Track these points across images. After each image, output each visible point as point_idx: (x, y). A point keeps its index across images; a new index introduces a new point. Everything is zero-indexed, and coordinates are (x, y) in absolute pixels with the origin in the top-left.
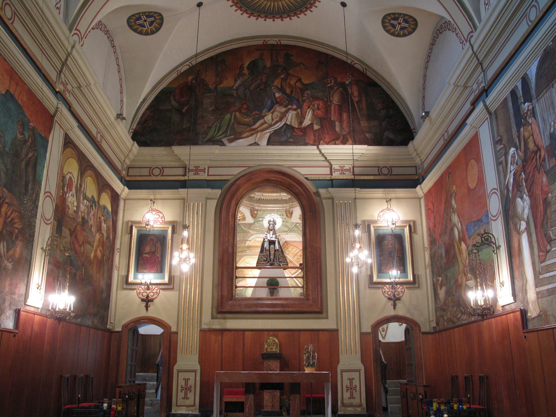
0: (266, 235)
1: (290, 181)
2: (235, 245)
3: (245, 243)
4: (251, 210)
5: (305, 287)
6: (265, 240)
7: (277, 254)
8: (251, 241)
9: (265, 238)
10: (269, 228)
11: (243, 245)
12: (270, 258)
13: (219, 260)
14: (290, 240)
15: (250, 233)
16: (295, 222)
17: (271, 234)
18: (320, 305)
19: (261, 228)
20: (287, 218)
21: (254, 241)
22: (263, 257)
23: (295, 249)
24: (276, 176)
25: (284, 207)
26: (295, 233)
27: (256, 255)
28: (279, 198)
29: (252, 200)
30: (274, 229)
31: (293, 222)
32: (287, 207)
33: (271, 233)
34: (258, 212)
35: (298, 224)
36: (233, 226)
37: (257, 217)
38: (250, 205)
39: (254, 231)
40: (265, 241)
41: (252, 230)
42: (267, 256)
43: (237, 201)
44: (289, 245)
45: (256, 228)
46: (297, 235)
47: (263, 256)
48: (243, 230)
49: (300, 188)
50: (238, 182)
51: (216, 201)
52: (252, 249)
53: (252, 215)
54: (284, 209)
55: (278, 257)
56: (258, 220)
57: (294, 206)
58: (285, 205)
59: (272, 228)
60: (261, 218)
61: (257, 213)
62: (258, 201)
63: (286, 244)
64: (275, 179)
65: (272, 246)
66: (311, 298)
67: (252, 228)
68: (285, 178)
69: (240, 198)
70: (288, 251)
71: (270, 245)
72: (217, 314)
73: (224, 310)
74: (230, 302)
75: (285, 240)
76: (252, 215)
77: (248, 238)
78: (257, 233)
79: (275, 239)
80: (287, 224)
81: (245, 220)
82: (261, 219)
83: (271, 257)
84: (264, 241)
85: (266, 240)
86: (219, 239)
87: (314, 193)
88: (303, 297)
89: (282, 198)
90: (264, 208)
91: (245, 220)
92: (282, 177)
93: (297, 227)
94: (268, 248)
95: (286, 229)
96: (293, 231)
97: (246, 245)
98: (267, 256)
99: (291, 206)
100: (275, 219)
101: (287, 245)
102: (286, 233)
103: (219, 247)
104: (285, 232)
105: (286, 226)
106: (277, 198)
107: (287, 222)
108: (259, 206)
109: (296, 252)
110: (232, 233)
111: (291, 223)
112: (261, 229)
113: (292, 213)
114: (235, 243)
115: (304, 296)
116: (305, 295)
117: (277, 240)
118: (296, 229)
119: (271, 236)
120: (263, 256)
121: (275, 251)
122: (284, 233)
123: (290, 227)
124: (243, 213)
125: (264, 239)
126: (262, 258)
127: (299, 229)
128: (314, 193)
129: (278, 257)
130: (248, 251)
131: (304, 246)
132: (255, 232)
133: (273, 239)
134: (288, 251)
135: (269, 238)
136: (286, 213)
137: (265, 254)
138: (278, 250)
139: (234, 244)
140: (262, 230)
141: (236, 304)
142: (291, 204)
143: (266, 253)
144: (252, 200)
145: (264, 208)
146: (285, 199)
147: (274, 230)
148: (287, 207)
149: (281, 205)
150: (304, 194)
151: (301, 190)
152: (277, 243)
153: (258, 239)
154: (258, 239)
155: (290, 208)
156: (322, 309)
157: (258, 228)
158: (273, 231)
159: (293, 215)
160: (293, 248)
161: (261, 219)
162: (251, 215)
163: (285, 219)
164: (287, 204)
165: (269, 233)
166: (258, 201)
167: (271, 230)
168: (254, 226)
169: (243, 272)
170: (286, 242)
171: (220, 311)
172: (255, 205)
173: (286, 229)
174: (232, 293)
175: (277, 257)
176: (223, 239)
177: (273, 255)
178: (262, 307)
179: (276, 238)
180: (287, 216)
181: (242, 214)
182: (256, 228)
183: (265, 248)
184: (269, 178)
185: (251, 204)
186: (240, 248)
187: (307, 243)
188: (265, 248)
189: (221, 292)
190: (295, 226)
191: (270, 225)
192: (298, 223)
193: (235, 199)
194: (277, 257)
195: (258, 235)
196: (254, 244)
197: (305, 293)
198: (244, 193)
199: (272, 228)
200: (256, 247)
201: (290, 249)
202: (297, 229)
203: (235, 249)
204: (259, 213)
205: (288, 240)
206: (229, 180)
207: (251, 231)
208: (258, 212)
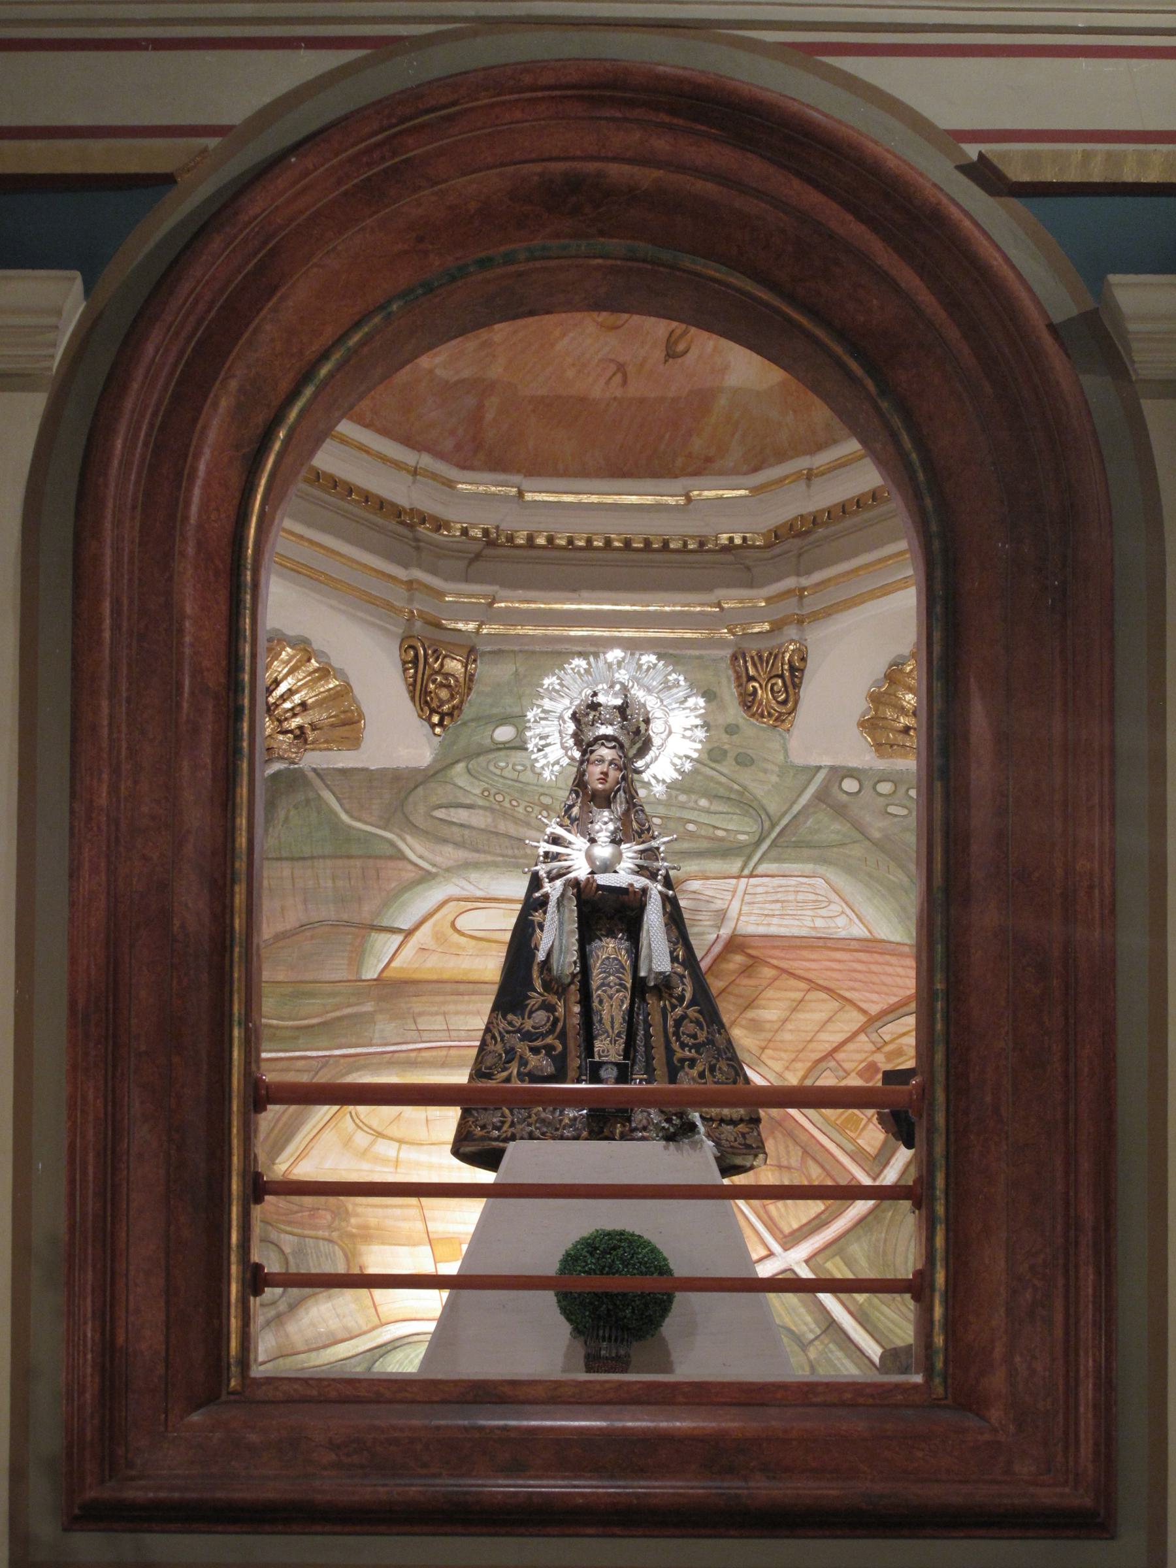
0: (556, 840)
1: (813, 198)
2: (241, 865)
3: (358, 956)
4: (408, 643)
5: (940, 1278)
6: (547, 887)
7: (656, 1018)
8: (409, 933)
9: (542, 869)
10: (580, 784)
11: (336, 970)
12: (590, 1051)
13: (73, 1003)
14: (776, 927)
15: (403, 857)
16: (827, 761)
17: (603, 837)
18: (1086, 1450)
19: (504, 814)
20: (751, 728)
21: (439, 937)
22: (522, 1048)
23: (820, 1009)
24: (661, 144)
25: (722, 618)
26: (825, 861)
27: (460, 1066)
28: (674, 529)
29: (418, 544)
30: (631, 797)
31: (799, 757)
32: (755, 615)
33: (604, 823)
34: (481, 669)
35: (850, 785)
36: (215, 679)
37: (468, 712)
38: (398, 597)
39: (445, 841)
40: (543, 902)
41: (414, 829)
42: (563, 1037)
43: (260, 418)
44: (768, 972)
45: (461, 815)
46: (842, 881)
47: (527, 1036)
48: (336, 827)
49: (908, 277)
50: (257, 205)
51: (36, 404)
52: (417, 1005)
53: (425, 692)
54: (722, 643)
55: (670, 1052)
56: (480, 737)
57: (813, 604)
58: (732, 599)
59: (614, 775)
60: (504, 720)
61: (470, 678)
62: (478, 556)
63: (739, 959)
64: (647, 177)
65: (609, 949)
66: (997, 1381)
67: (419, 819)
68: (756, 168)
69: (285, 385)
70: (756, 1026)
71: (587, 935)
72: (66, 1529)
73: (132, 1494)
74: (195, 1417)
75: (725, 932)
76: (421, 696)
77: (379, 913)
78: (467, 866)
79: (640, 882)
80: (746, 777)
81: (354, 742)
82: (504, 733)
83: (598, 1045)
84: (534, 904)
85: (553, 889)
86: (73, 795)
87: (1052, 328)
88: (918, 1379)
89: (704, 531)
90: (529, 631)
91: (354, 742)
92: (725, 157)
93: (840, 811)
94: (567, 962)
95: (741, 829)
96: (798, 845)
97: (371, 972)
98: (563, 1037)
99: (790, 607)
100: (638, 694)
101: (747, 971)
102: (735, 866)
103: (74, 873)
104: (724, 850)
105: (745, 803)
106: (657, 527)
107: (744, 761)
108: (487, 613)
109: (831, 1038)
110: (206, 739)
111: (787, 768)
112: (503, 826)
113: (795, 675)
114: (242, 840)
115: (929, 1372)
116: (939, 1364)
117: (656, 888)
118: (834, 829)
119: (603, 851)
120: (527, 1036)
121: (640, 988)
122: (714, 866)
123: (773, 808)
124: (340, 674)
125: (536, 882)
126: (510, 1052)
127: (858, 826)
128: (1052, 328)
129: (670, 1052)
130: (385, 1027)
131: (938, 881)
132: (449, 855)
133: (623, 877)
134: (756, 1026)
135: (581, 871)
136: (744, 679)
137: (541, 1016)
138: (664, 985)
139: (224, 849)
140: (513, 830)
141: (253, 1437)
142: (790, 582)
143: (550, 1008)
144: (418, 544)
145: (529, 631)
146: (730, 548)
147: (632, 802)
148: (755, 615)
149: (696, 604)
150: (953, 333)
151: (925, 297)
152: (654, 918)
153: (473, 921)
154: (473, 921)
155: (777, 626)
156: (1106, 1488)
157: (479, 819)
158: (619, 807)
159: (809, 692)
160: (797, 1006)
161: (504, 733)
162: (412, 687)
163: (731, 730)
164: (751, 584)
165: (582, 825)
166: (478, 556)
167: (604, 800)
168: (441, 793)
169: (346, 1215)
170: (735, 944)
171: (91, 1494)
172: (456, 593)
173: (741, 829)
174: (219, 1336)
175: (659, 1054)
176: (114, 789)
177: (619, 1025)
178: (516, 1468)
179: (653, 876)
180: (748, 701)
181: (324, 672)
182: (461, 815)
183: (546, 964)
184: (592, 167)
185: (410, 584)
186: (312, 995)
187: (974, 848)
188: (546, 964)
189: (106, 1315)
190: (822, 796)
191: (586, 745)
192: (851, 773)
193: (233, 384)
194: (659, 1054)
195: (474, 875)
196: (438, 965)
197: (939, 1340)
198: (329, 333)
199: (614, 775)
200: (460, 987)
201: (770, 1014)
202: (836, 826)
203: (239, 899)
204: (490, 673)
205: (751, 926)
206: (167, 180)
207: (413, 848)
208: (481, 669)
